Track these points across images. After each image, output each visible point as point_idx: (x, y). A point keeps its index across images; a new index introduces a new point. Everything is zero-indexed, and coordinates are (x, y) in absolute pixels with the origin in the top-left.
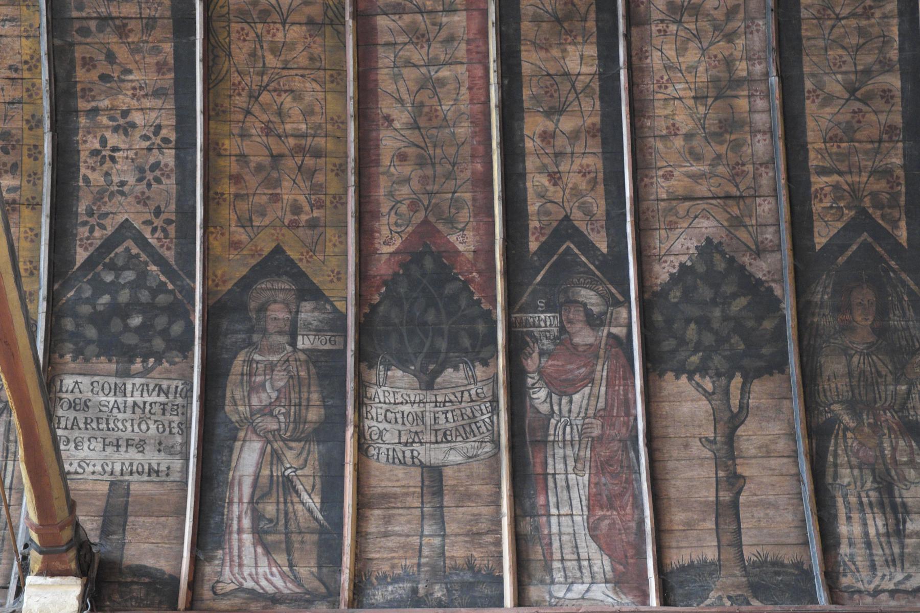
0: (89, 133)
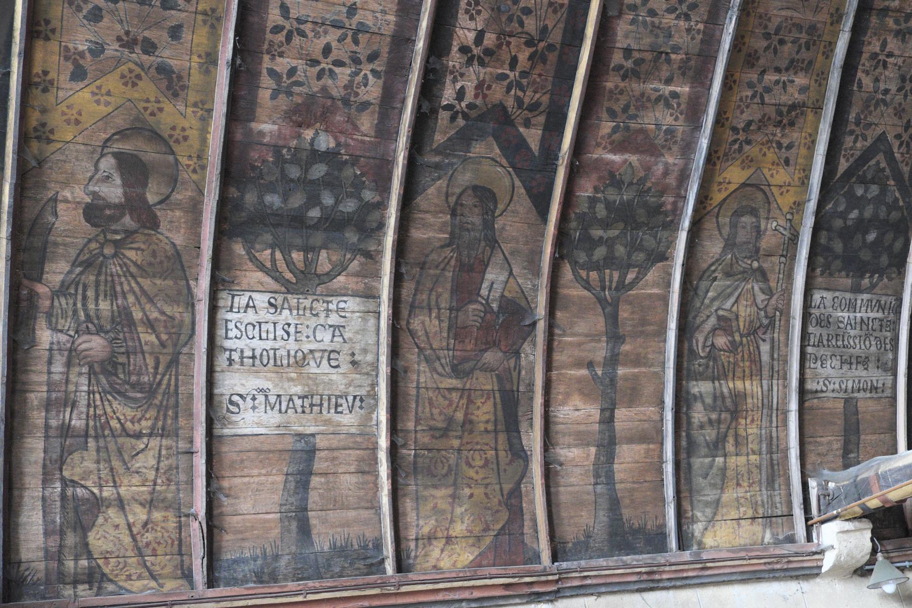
0: (875, 34)
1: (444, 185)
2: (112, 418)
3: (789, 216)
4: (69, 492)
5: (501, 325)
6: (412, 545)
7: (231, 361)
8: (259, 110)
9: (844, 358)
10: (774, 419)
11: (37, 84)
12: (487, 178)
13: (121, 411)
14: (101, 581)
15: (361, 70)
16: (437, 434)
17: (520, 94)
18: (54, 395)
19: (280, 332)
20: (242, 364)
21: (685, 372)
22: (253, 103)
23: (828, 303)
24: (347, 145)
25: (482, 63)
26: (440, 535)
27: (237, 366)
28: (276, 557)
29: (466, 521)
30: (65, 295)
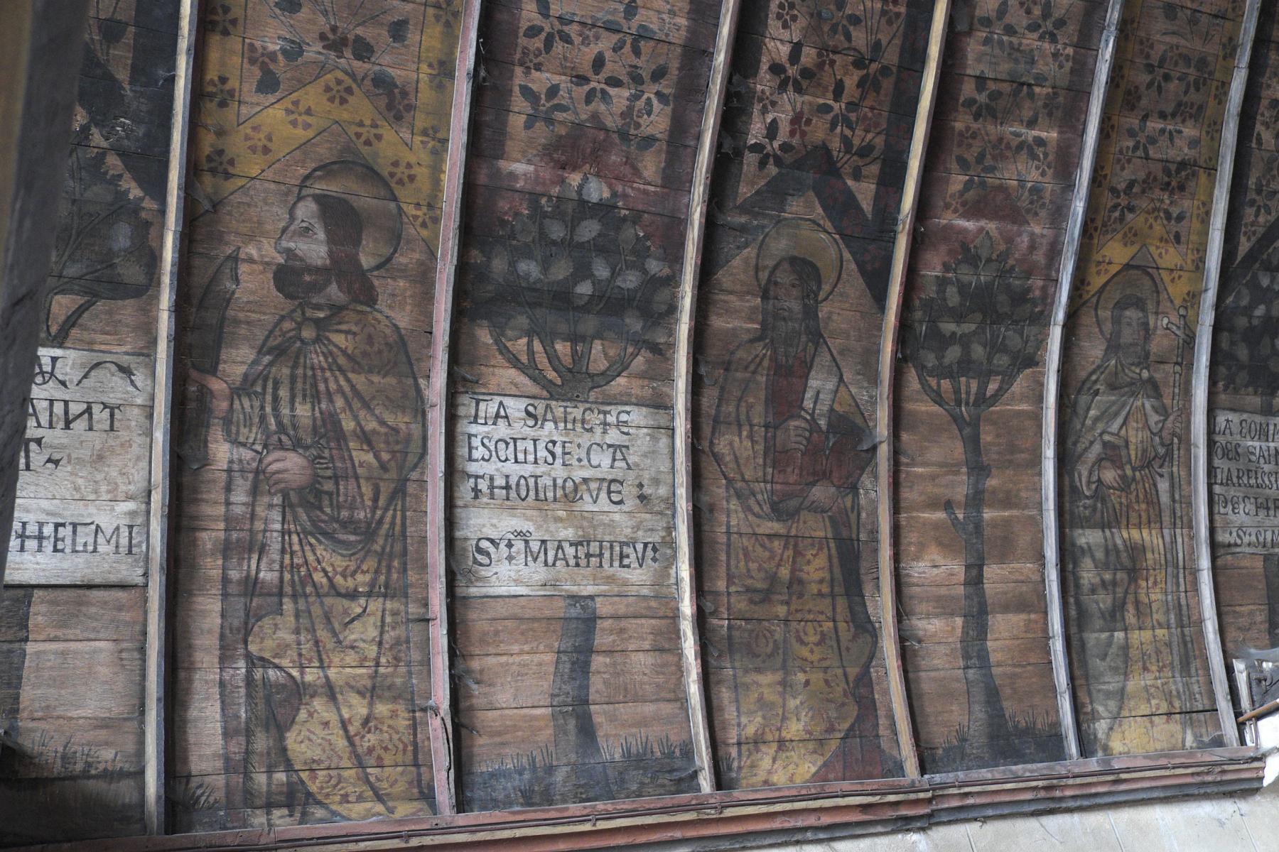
1: (754, 254)
2: (316, 569)
3: (1182, 312)
4: (258, 674)
5: (832, 450)
6: (734, 752)
7: (477, 492)
8: (509, 143)
9: (1260, 501)
10: (1181, 580)
11: (211, 96)
12: (810, 244)
13: (328, 560)
14: (306, 804)
15: (643, 92)
16: (757, 598)
17: (848, 132)
18: (235, 535)
19: (542, 453)
20: (492, 497)
21: (1067, 516)
22: (502, 132)
23: (1236, 429)
24: (625, 196)
25: (799, 90)
26: (769, 737)
27: (485, 500)
28: (550, 770)
29: (803, 718)
30: (249, 395)
